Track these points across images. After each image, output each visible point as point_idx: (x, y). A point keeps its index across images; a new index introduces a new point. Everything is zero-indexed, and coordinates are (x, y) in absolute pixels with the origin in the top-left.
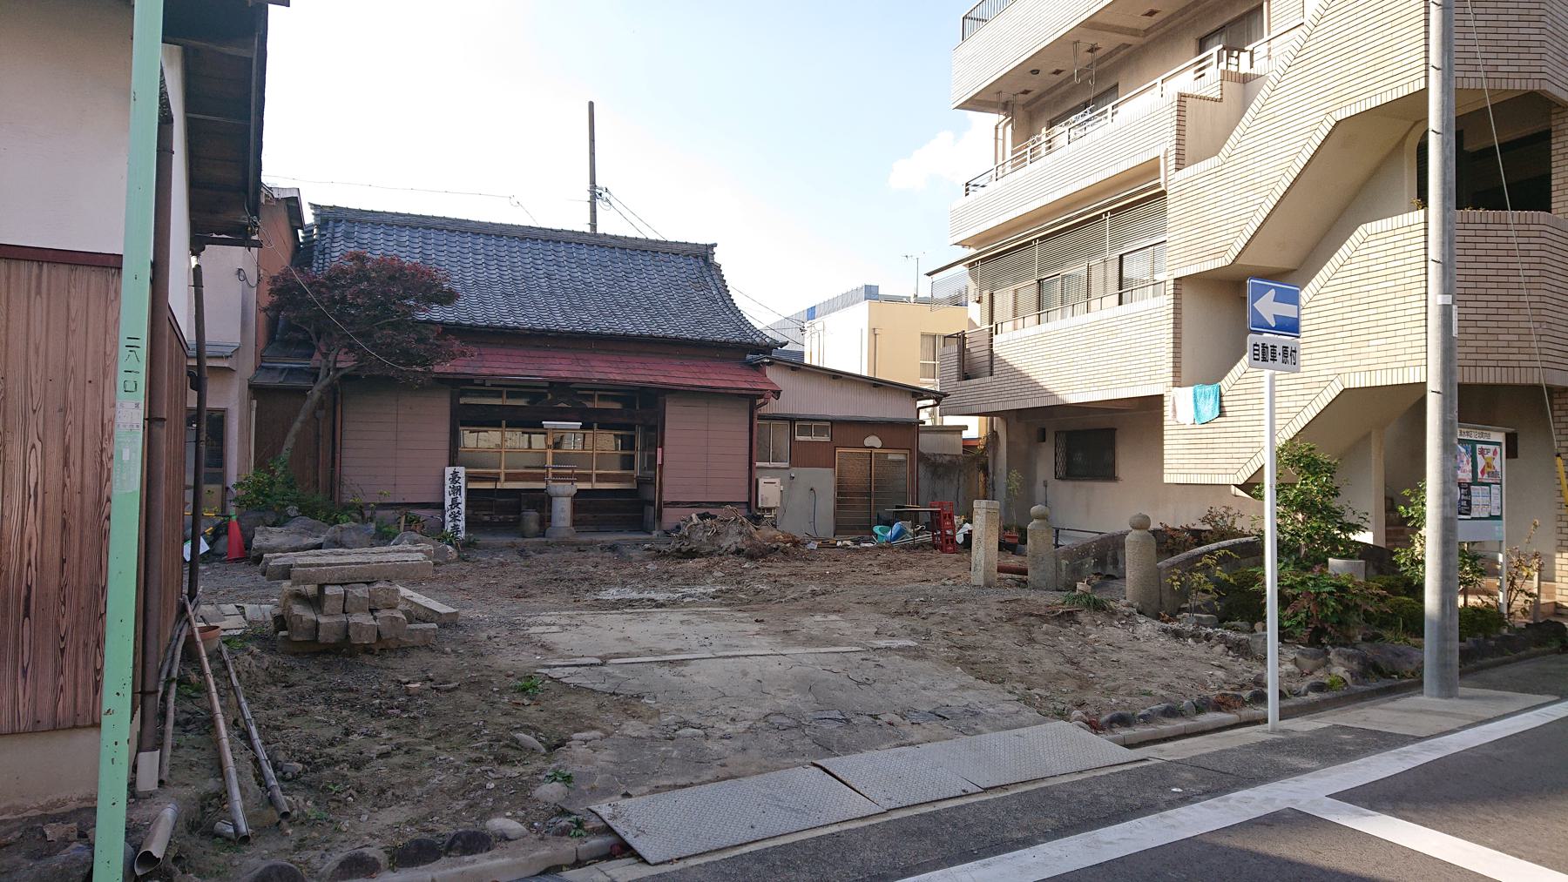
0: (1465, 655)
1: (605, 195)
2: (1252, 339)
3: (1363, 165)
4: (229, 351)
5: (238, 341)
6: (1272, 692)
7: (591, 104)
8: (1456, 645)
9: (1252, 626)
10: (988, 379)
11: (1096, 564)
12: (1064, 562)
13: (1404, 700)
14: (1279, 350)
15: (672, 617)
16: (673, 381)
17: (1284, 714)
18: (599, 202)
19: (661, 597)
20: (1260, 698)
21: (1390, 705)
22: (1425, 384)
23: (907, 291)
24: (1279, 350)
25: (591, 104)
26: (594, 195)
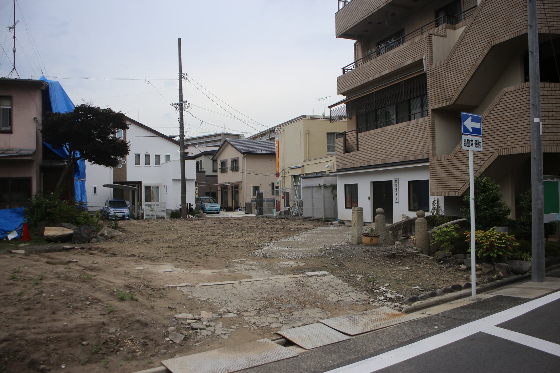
0: (547, 264)
1: (186, 77)
2: (464, 137)
3: (506, 58)
4: (31, 152)
5: (34, 148)
6: (473, 283)
7: (180, 39)
8: (544, 260)
9: (465, 256)
10: (356, 152)
11: (403, 233)
12: (390, 232)
13: (524, 284)
14: (474, 142)
15: (42, 259)
16: (325, 228)
17: (478, 292)
18: (183, 80)
19: (67, 247)
20: (469, 286)
21: (518, 286)
22: (530, 153)
23: (319, 114)
24: (474, 142)
25: (180, 39)
26: (181, 77)
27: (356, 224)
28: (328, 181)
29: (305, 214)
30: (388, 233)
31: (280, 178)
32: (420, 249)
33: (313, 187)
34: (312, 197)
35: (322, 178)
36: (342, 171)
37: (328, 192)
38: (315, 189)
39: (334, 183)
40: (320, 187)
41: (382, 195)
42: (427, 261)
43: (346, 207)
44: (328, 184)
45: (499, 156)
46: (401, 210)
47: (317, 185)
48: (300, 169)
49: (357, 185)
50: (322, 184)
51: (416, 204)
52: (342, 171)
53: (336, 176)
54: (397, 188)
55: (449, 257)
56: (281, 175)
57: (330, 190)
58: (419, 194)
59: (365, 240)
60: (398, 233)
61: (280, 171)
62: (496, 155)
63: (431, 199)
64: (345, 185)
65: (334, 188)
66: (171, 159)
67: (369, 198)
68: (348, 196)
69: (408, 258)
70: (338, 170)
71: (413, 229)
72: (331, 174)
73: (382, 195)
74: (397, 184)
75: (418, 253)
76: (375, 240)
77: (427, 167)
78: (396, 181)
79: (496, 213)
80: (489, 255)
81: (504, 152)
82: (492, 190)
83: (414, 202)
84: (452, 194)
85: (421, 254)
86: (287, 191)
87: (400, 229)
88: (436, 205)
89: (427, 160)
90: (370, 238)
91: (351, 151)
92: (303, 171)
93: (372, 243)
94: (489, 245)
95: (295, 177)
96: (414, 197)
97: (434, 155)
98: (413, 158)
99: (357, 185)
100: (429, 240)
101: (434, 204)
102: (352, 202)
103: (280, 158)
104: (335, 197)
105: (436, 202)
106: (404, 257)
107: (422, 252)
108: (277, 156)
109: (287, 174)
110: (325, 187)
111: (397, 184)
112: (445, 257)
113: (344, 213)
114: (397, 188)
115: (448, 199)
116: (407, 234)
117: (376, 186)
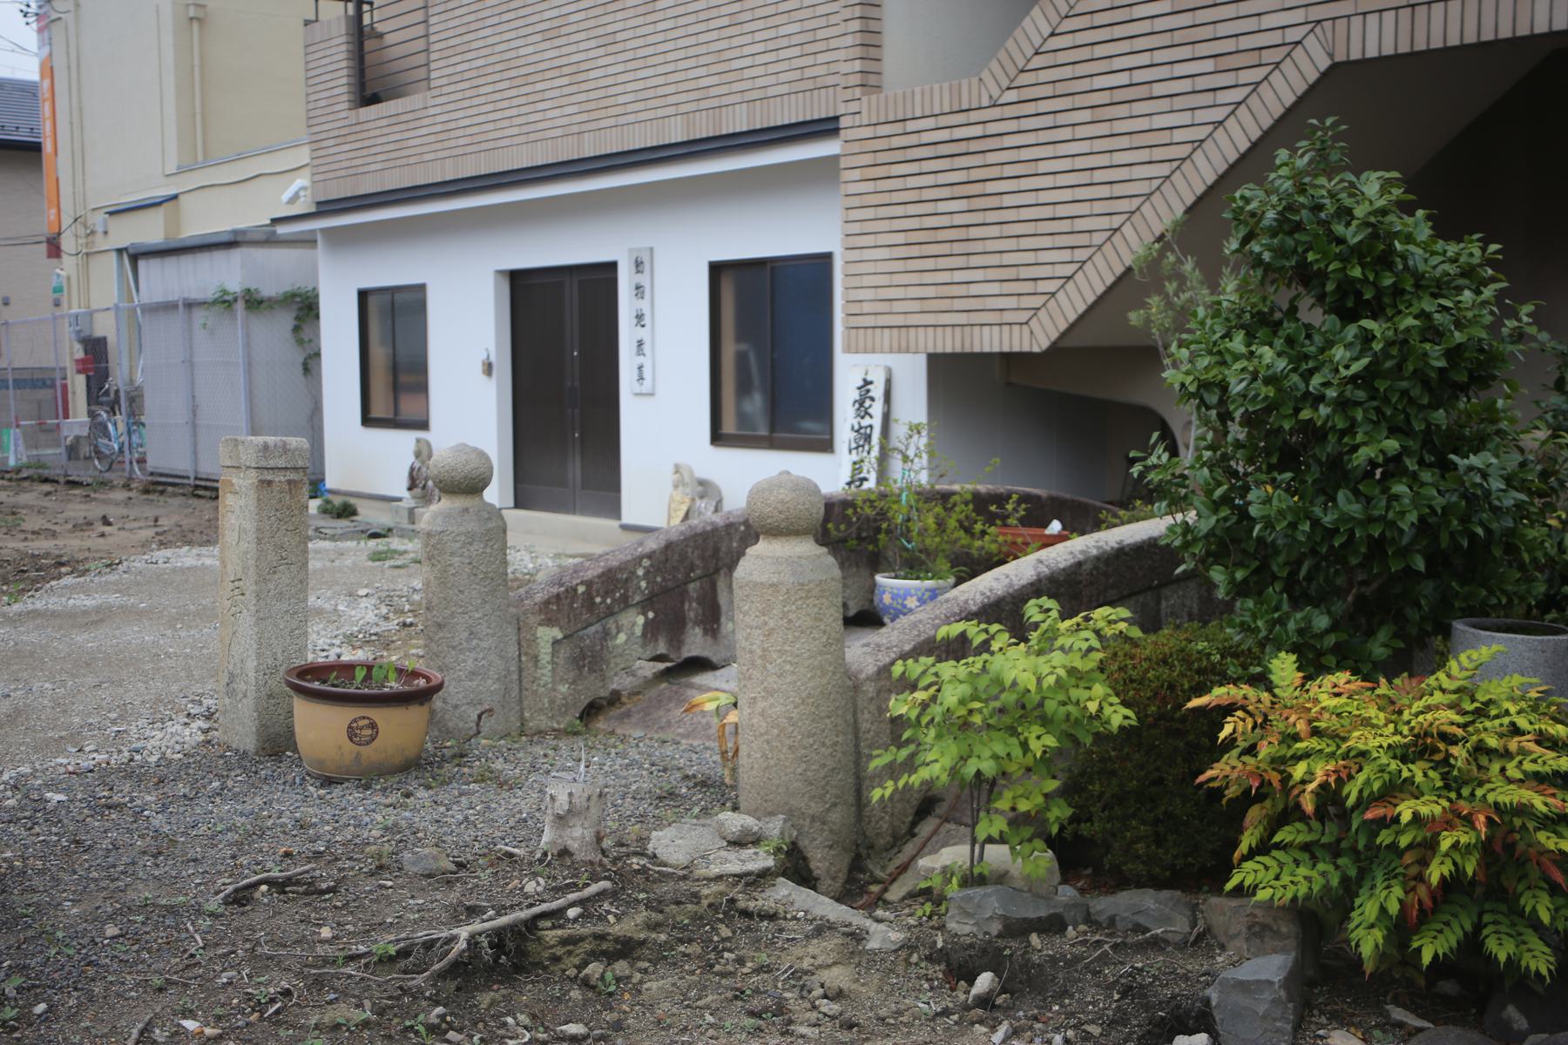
11: (651, 630)
12: (547, 635)
27: (249, 586)
28: (273, 271)
29: (155, 462)
30: (525, 646)
31: (68, 266)
32: (774, 827)
33: (190, 305)
34: (190, 364)
35: (236, 255)
36: (344, 211)
37: (275, 331)
38: (199, 316)
39: (303, 284)
40: (225, 302)
41: (564, 346)
42: (838, 977)
43: (368, 420)
44: (269, 290)
45: (1335, 67)
46: (670, 442)
47: (210, 294)
48: (161, 210)
49: (421, 288)
50: (235, 286)
51: (756, 404)
52: (344, 211)
53: (308, 241)
54: (644, 305)
55: (1053, 925)
56: (67, 244)
57: (286, 320)
58: (773, 341)
59: (320, 728)
60: (606, 635)
61: (66, 221)
62: (1311, 63)
63: (850, 371)
64: (363, 295)
65: (306, 308)
66: (43, 248)
67: (488, 369)
68: (379, 353)
69: (661, 956)
70: (326, 208)
71: (723, 599)
72: (282, 230)
73: (564, 346)
74: (644, 279)
75: (759, 879)
76: (398, 729)
77: (829, 166)
78: (638, 264)
79: (1476, 500)
80: (1472, 944)
81: (1377, 39)
82: (1440, 287)
83: (744, 388)
84: (990, 341)
85: (784, 889)
86: (98, 333)
87: (625, 603)
88: (877, 409)
89: (826, 128)
90: (349, 714)
91: (395, 93)
92: (174, 222)
93: (369, 753)
94: (1486, 847)
95: (135, 256)
96: (741, 359)
97: (869, 83)
98: (738, 121)
99: (421, 288)
100: (859, 759)
101: (862, 407)
102: (396, 389)
103: (61, 161)
104: (311, 364)
105: (877, 391)
106: (626, 949)
107: (796, 867)
108: (48, 148)
109: (101, 244)
110: (254, 302)
111: (644, 279)
112: (1017, 929)
113: (365, 460)
114: (644, 305)
115: (952, 376)
116: (676, 640)
117: (525, 288)
